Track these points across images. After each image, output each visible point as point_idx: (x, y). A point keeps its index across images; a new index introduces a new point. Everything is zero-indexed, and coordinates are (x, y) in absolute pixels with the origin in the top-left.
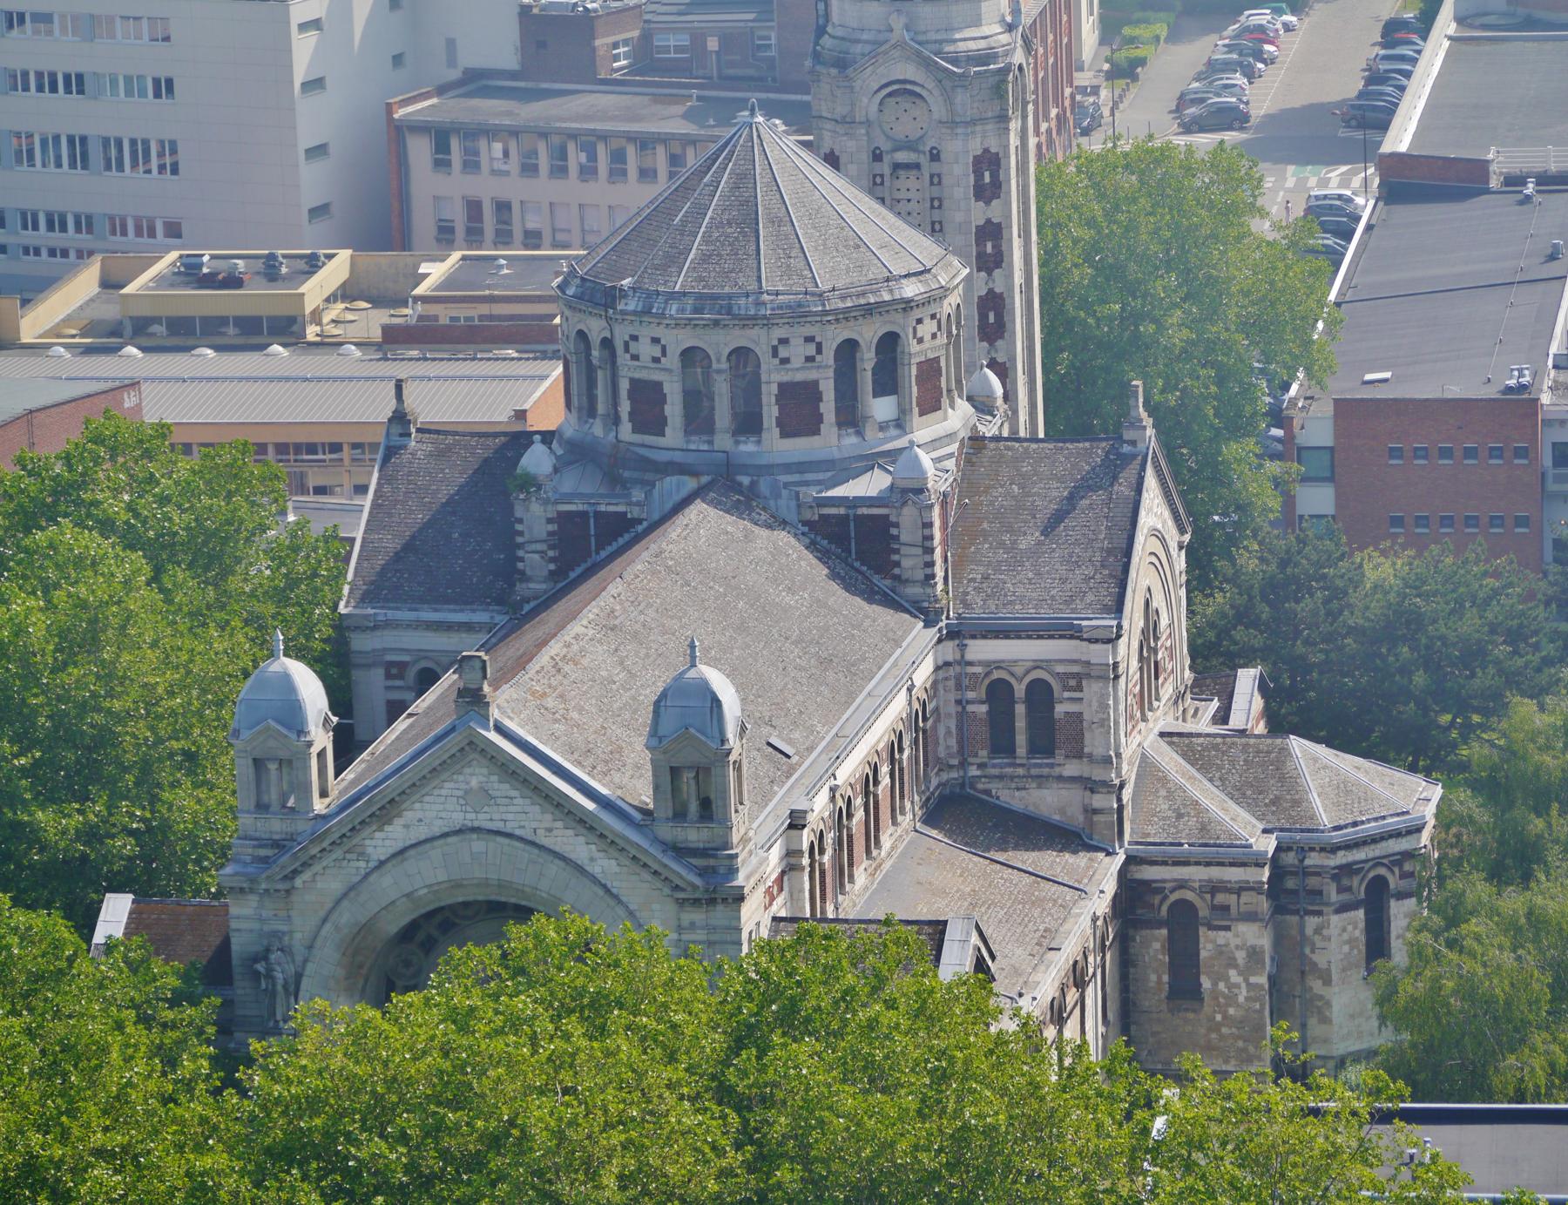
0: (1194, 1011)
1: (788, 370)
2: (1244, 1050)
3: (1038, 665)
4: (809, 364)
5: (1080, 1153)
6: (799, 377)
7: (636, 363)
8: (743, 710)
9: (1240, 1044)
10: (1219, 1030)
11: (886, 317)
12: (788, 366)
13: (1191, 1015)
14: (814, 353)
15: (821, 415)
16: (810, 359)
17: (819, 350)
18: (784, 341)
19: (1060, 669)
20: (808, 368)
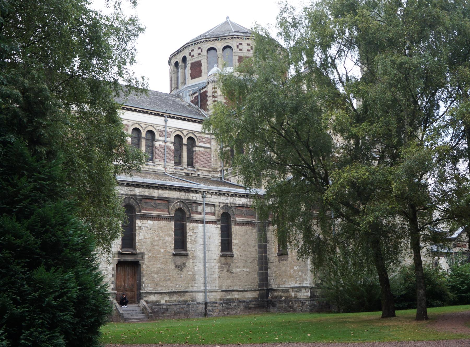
0: (286, 260)
1: (194, 59)
2: (301, 276)
3: (192, 132)
4: (199, 56)
5: (186, 275)
6: (196, 60)
7: (241, 51)
8: (146, 151)
9: (300, 274)
10: (293, 268)
11: (226, 41)
12: (249, 52)
13: (285, 262)
14: (250, 49)
15: (202, 71)
16: (199, 54)
17: (202, 51)
18: (192, 50)
19: (159, 128)
20: (199, 57)
